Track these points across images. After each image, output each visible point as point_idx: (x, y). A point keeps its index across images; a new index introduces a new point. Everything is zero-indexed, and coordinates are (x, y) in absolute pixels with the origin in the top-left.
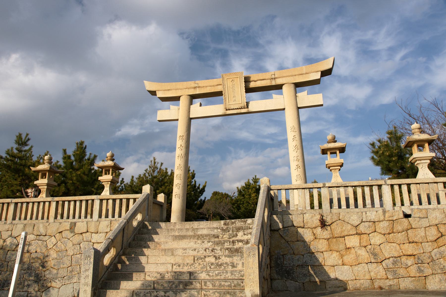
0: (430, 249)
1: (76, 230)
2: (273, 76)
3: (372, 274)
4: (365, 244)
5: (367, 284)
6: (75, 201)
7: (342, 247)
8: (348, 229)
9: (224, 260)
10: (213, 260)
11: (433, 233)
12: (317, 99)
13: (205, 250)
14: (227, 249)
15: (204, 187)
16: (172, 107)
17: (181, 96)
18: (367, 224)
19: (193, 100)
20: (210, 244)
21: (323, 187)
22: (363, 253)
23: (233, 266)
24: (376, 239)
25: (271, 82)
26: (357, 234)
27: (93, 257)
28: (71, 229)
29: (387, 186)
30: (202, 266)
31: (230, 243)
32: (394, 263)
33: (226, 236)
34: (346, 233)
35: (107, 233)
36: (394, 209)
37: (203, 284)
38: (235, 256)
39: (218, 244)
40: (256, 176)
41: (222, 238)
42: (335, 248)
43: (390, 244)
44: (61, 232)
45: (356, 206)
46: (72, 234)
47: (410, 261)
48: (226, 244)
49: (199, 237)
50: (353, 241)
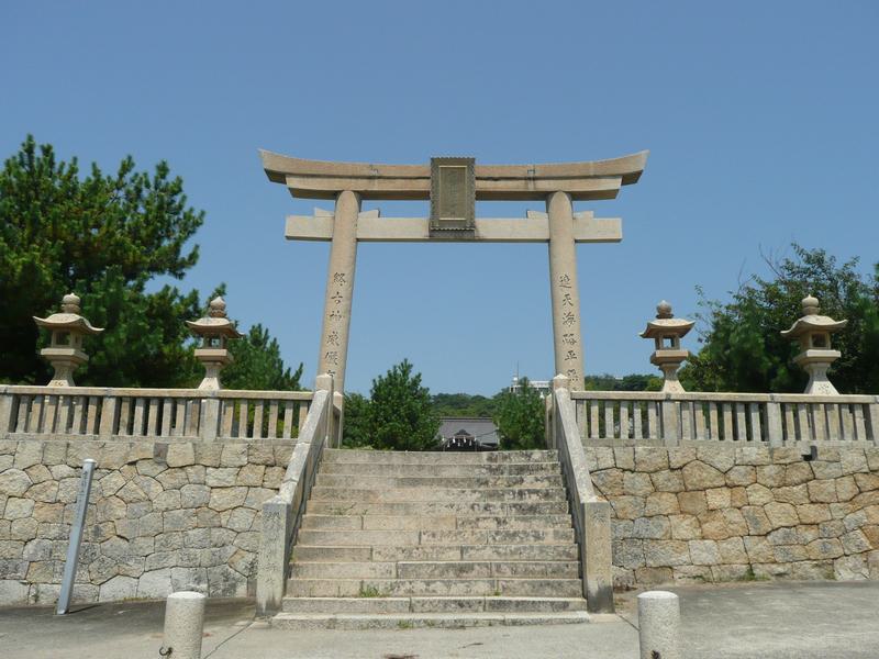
0: (840, 515)
1: (171, 459)
2: (531, 175)
3: (751, 554)
4: (739, 504)
5: (111, 600)
6: (100, 400)
7: (700, 507)
8: (709, 477)
9: (519, 526)
10: (493, 525)
11: (846, 488)
12: (612, 227)
13: (472, 507)
14: (515, 506)
15: (299, 373)
16: (317, 211)
17: (340, 192)
18: (742, 469)
19: (363, 201)
20: (477, 495)
21: (666, 400)
22: (735, 516)
23: (537, 537)
24: (759, 496)
25: (527, 184)
26: (726, 485)
27: (285, 515)
28: (157, 456)
29: (775, 405)
30: (479, 535)
31: (514, 494)
32: (787, 536)
33: (501, 485)
34: (708, 484)
35: (241, 467)
36: (784, 445)
37: (494, 569)
38: (535, 518)
39: (491, 495)
40: (406, 360)
41: (495, 484)
42: (690, 508)
43: (779, 506)
44: (134, 463)
45: (735, 437)
46: (161, 468)
47: (810, 534)
48: (506, 496)
49: (449, 482)
50: (718, 499)
